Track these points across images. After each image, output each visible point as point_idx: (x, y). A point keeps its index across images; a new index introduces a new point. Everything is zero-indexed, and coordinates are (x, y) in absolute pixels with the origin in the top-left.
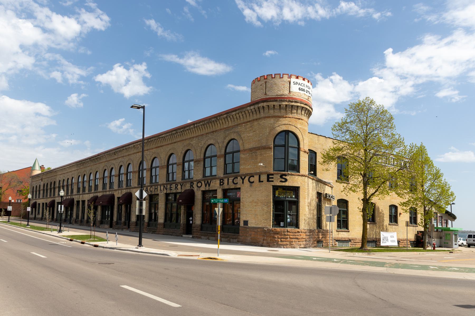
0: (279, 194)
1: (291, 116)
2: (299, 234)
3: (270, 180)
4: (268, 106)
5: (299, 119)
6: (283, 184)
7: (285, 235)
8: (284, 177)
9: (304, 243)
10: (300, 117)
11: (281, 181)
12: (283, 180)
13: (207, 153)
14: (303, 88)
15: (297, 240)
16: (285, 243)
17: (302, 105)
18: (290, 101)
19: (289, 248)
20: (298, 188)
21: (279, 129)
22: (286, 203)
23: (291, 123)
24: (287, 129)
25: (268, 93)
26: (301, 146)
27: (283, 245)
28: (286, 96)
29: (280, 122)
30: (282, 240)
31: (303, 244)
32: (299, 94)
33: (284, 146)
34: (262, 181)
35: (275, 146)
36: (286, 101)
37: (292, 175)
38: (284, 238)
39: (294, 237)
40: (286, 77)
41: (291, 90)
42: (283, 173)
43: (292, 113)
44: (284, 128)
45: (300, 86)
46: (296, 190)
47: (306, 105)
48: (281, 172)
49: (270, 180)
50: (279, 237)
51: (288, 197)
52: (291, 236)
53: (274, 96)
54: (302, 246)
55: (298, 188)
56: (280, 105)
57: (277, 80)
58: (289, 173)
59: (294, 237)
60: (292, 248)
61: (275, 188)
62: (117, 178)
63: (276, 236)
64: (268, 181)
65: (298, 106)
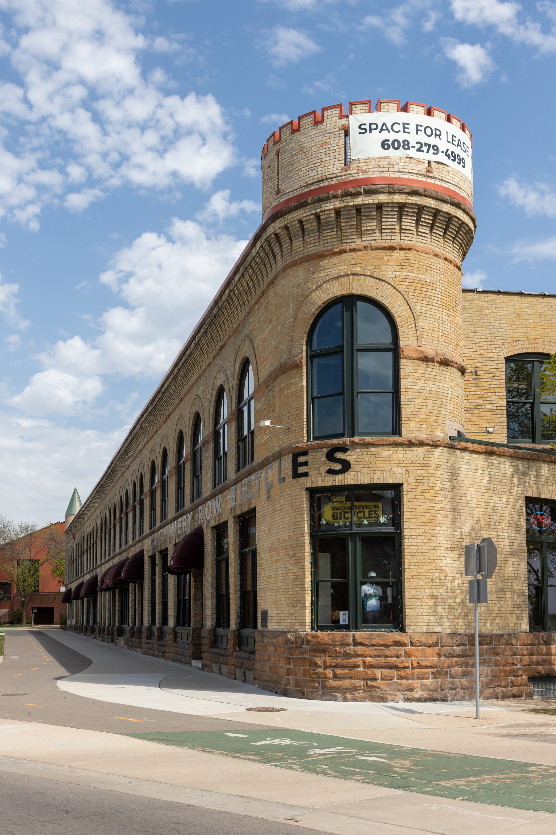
0: (335, 516)
1: (358, 243)
2: (402, 651)
3: (301, 470)
4: (286, 227)
5: (392, 248)
6: (338, 480)
7: (347, 655)
8: (339, 455)
9: (429, 682)
10: (394, 243)
11: (331, 472)
12: (338, 467)
13: (178, 425)
14: (401, 137)
15: (394, 672)
16: (346, 683)
17: (398, 198)
18: (346, 194)
19: (363, 699)
20: (397, 488)
21: (320, 298)
22: (350, 544)
23: (358, 270)
24: (345, 292)
25: (282, 187)
26: (403, 342)
27: (344, 690)
28: (335, 181)
29: (322, 274)
30: (338, 671)
31: (425, 688)
32: (383, 163)
33: (339, 351)
34: (417, 133)
35: (312, 357)
36: (335, 197)
37: (368, 445)
38: (343, 667)
39: (382, 660)
40: (332, 120)
41: (353, 155)
42: (335, 441)
43: (361, 234)
44: (336, 290)
45: (385, 135)
46: (389, 496)
47: (415, 193)
48: (329, 442)
49: (301, 470)
50: (329, 661)
51: (360, 525)
52: (368, 659)
53: (299, 192)
54: (418, 694)
55: (397, 488)
56: (318, 217)
57: (309, 135)
58: (356, 439)
59: (382, 660)
60: (373, 699)
61: (318, 497)
62: (229, 638)
63: (319, 661)
64: (296, 475)
65: (380, 207)
